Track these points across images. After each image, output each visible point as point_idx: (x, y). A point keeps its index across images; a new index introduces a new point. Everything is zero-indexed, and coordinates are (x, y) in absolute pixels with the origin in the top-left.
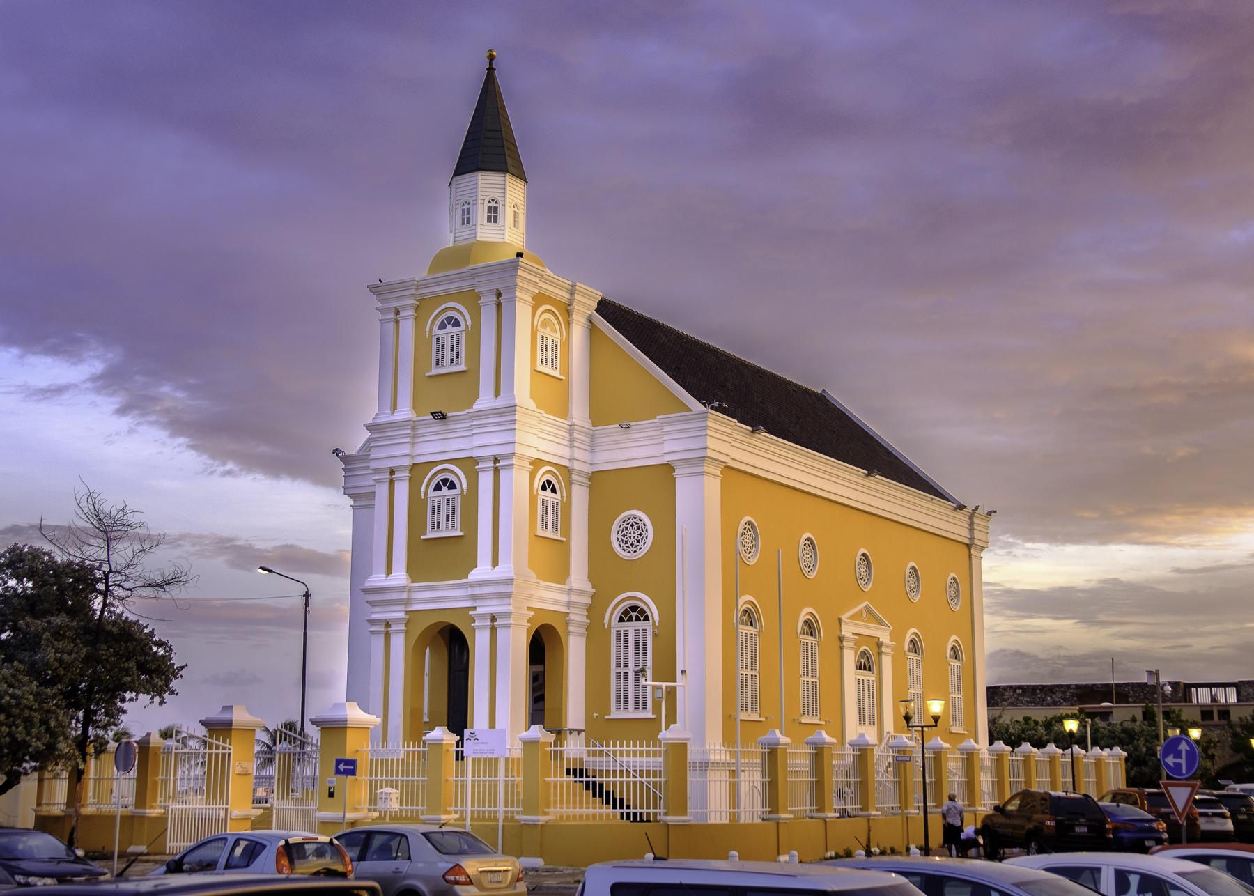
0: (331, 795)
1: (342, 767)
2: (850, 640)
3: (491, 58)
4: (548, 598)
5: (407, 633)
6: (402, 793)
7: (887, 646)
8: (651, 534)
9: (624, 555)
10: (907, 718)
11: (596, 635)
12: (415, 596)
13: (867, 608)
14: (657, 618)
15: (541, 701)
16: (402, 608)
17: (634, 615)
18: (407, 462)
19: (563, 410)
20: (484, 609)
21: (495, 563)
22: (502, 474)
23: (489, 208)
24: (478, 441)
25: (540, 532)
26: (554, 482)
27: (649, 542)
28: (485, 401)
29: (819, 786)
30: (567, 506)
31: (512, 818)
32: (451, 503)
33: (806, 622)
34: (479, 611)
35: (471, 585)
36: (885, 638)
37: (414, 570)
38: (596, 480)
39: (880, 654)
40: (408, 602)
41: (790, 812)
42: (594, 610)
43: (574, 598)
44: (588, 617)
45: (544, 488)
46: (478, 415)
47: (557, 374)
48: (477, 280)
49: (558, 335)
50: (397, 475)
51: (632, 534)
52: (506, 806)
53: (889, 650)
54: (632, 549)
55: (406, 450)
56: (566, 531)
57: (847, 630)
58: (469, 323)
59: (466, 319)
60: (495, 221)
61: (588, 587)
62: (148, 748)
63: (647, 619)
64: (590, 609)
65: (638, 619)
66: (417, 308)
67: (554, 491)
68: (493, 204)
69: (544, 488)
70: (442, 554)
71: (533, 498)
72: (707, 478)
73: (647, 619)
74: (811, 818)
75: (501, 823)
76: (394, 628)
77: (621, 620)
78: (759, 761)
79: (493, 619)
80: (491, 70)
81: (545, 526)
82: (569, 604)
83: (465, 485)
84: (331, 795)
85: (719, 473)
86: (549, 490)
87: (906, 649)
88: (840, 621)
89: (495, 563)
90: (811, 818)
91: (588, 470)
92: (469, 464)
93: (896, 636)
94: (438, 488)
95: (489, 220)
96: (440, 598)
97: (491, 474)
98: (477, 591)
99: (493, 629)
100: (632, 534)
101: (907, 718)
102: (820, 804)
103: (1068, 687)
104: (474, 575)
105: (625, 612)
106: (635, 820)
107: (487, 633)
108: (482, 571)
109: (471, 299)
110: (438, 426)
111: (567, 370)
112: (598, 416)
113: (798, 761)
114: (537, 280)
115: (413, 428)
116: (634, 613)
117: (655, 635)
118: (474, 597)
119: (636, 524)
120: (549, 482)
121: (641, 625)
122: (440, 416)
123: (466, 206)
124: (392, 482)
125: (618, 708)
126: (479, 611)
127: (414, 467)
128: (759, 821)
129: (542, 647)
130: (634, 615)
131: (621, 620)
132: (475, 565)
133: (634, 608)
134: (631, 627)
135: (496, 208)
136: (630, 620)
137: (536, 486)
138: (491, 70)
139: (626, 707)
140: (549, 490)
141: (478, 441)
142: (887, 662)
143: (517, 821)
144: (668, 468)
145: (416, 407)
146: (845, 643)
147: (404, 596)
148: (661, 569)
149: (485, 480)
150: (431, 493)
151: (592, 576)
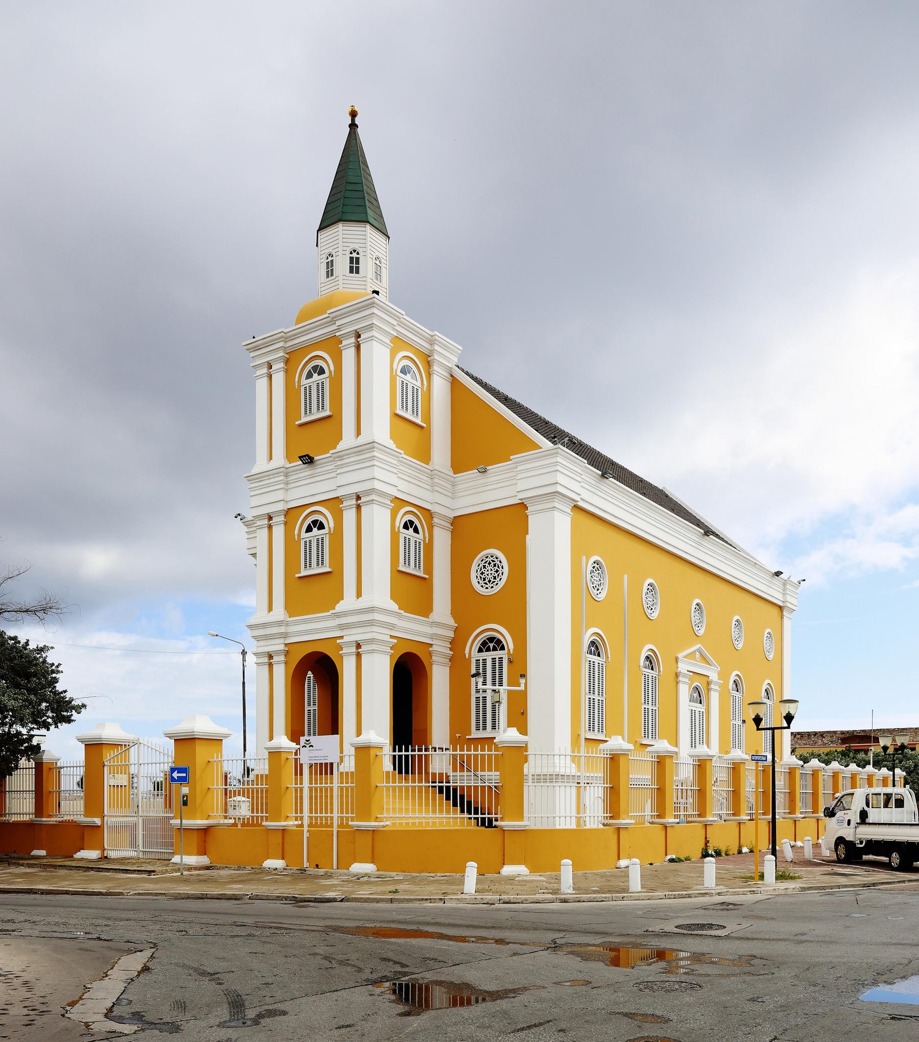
0: (185, 803)
1: (175, 775)
2: (685, 676)
3: (353, 114)
4: (415, 629)
5: (286, 663)
6: (253, 804)
7: (716, 683)
8: (506, 570)
9: (482, 591)
10: (757, 720)
11: (457, 662)
12: (292, 629)
13: (699, 650)
14: (511, 647)
15: (407, 724)
16: (281, 641)
17: (491, 645)
18: (282, 507)
19: (423, 453)
20: (352, 636)
21: (359, 594)
22: (364, 509)
23: (351, 259)
24: (342, 480)
25: (402, 568)
26: (416, 522)
27: (504, 578)
28: (348, 440)
29: (661, 792)
30: (429, 547)
31: (348, 826)
32: (320, 542)
33: (647, 658)
34: (346, 639)
35: (338, 615)
36: (714, 676)
37: (291, 607)
38: (458, 524)
39: (709, 690)
40: (285, 635)
41: (631, 817)
42: (457, 643)
43: (436, 630)
44: (451, 649)
45: (406, 527)
46: (340, 456)
47: (418, 421)
48: (338, 323)
49: (419, 384)
50: (274, 520)
51: (490, 572)
52: (311, 812)
53: (717, 688)
54: (490, 585)
55: (280, 495)
56: (429, 568)
57: (683, 667)
58: (332, 368)
59: (329, 365)
60: (357, 272)
61: (451, 622)
62: (42, 763)
63: (503, 648)
64: (453, 642)
65: (495, 649)
66: (287, 362)
67: (416, 530)
68: (354, 255)
69: (406, 527)
70: (313, 586)
71: (395, 536)
72: (557, 514)
73: (503, 648)
74: (652, 823)
75: (335, 829)
76: (275, 659)
77: (480, 650)
78: (601, 775)
79: (358, 646)
80: (353, 126)
81: (407, 562)
82: (433, 636)
83: (332, 525)
84: (185, 803)
85: (569, 511)
86: (411, 530)
87: (730, 688)
88: (677, 659)
89: (359, 594)
90: (652, 823)
91: (452, 515)
92: (334, 504)
93: (723, 675)
94: (309, 529)
95: (351, 271)
96: (312, 629)
97: (354, 510)
98: (343, 620)
99: (359, 655)
100: (490, 572)
101: (757, 720)
102: (660, 810)
103: (835, 732)
104: (340, 607)
105: (484, 643)
106: (483, 824)
107: (353, 659)
108: (349, 601)
109: (333, 344)
110: (307, 471)
111: (427, 417)
112: (458, 465)
113: (640, 775)
114: (395, 323)
115: (286, 475)
116: (492, 644)
117: (510, 662)
118: (341, 627)
119: (494, 563)
120: (411, 522)
121: (498, 654)
122: (308, 460)
123: (330, 259)
124: (270, 527)
125: (478, 729)
126: (346, 639)
127: (288, 512)
128: (601, 826)
129: (408, 675)
130: (491, 645)
131: (480, 650)
132: (341, 598)
133: (491, 639)
134: (489, 656)
135: (358, 259)
136: (488, 650)
137: (397, 524)
138: (353, 126)
139: (485, 728)
140: (411, 530)
141: (342, 480)
142: (715, 697)
143: (352, 827)
144: (522, 506)
145: (289, 457)
146: (680, 679)
147: (282, 629)
148: (513, 604)
149: (349, 517)
150: (304, 535)
151: (455, 612)
